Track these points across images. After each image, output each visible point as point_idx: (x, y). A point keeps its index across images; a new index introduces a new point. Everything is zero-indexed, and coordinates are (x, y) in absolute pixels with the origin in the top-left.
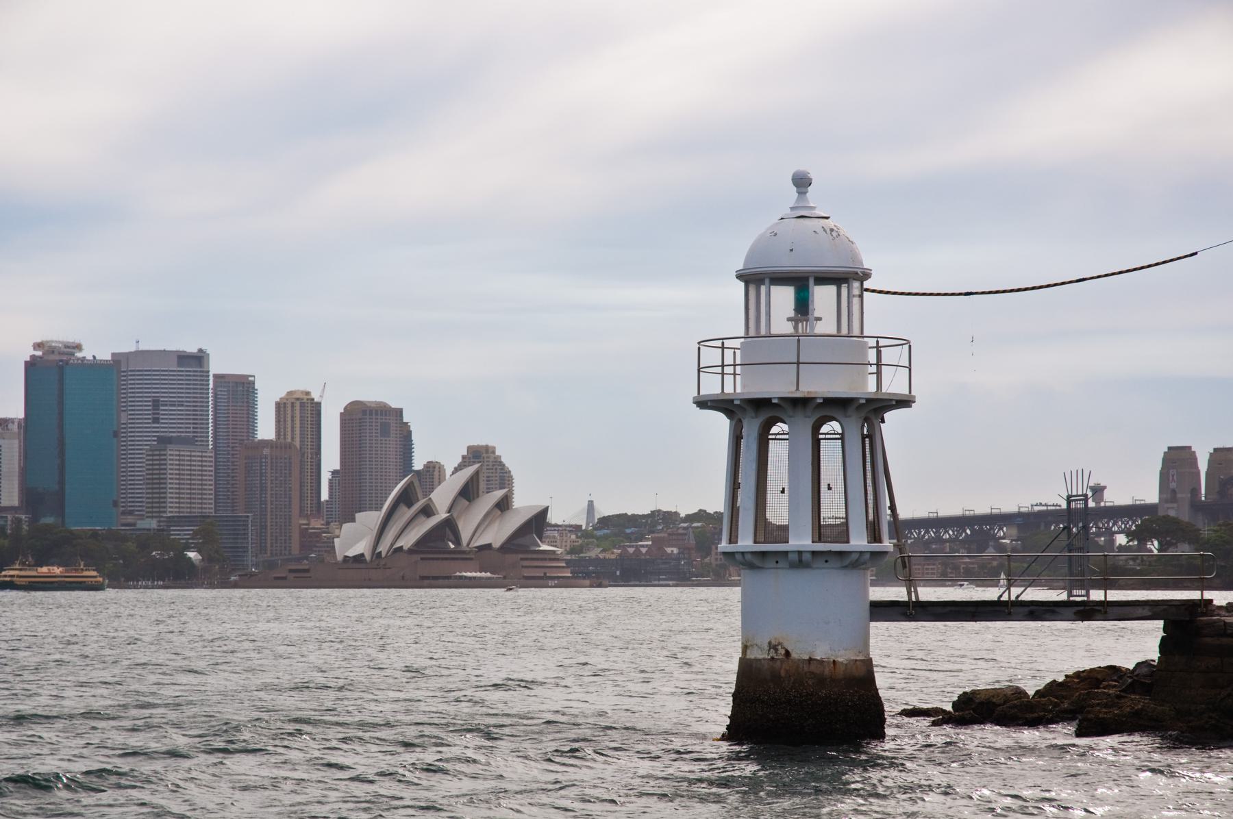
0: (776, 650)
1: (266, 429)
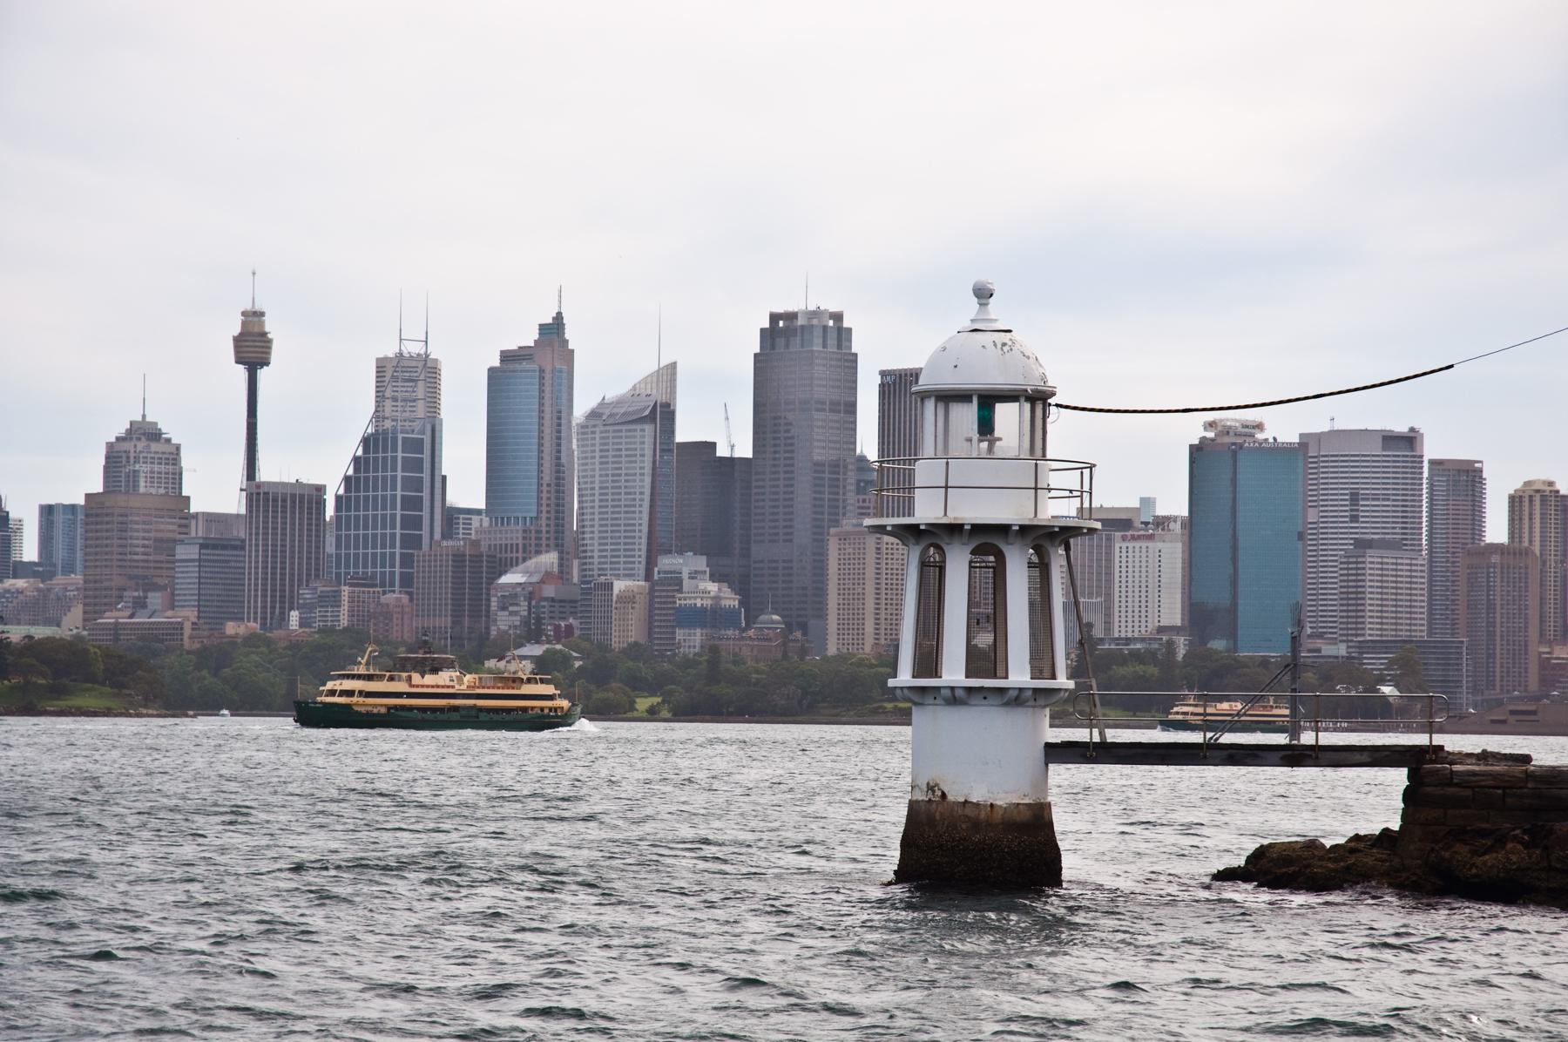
1: (1496, 529)
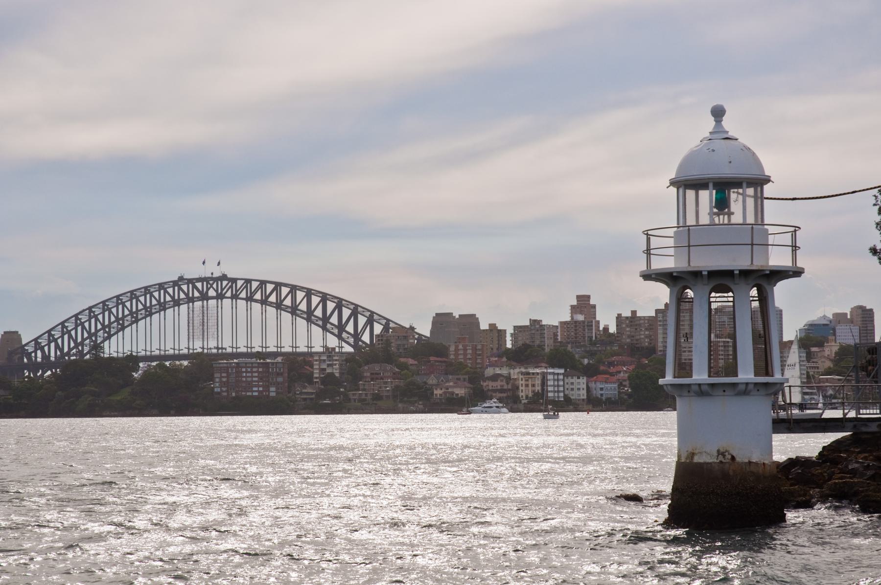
0: (724, 456)
